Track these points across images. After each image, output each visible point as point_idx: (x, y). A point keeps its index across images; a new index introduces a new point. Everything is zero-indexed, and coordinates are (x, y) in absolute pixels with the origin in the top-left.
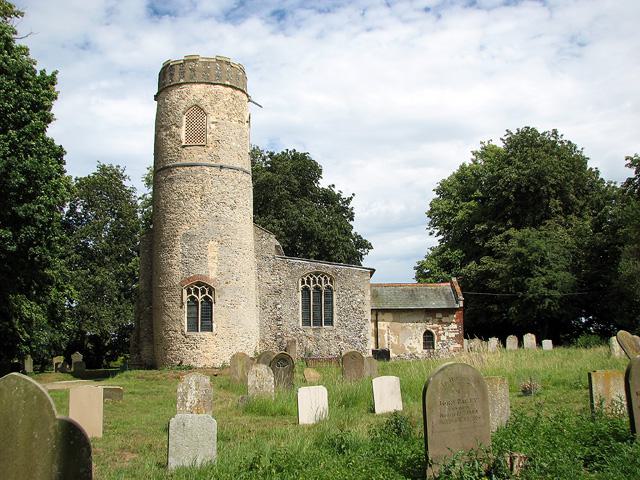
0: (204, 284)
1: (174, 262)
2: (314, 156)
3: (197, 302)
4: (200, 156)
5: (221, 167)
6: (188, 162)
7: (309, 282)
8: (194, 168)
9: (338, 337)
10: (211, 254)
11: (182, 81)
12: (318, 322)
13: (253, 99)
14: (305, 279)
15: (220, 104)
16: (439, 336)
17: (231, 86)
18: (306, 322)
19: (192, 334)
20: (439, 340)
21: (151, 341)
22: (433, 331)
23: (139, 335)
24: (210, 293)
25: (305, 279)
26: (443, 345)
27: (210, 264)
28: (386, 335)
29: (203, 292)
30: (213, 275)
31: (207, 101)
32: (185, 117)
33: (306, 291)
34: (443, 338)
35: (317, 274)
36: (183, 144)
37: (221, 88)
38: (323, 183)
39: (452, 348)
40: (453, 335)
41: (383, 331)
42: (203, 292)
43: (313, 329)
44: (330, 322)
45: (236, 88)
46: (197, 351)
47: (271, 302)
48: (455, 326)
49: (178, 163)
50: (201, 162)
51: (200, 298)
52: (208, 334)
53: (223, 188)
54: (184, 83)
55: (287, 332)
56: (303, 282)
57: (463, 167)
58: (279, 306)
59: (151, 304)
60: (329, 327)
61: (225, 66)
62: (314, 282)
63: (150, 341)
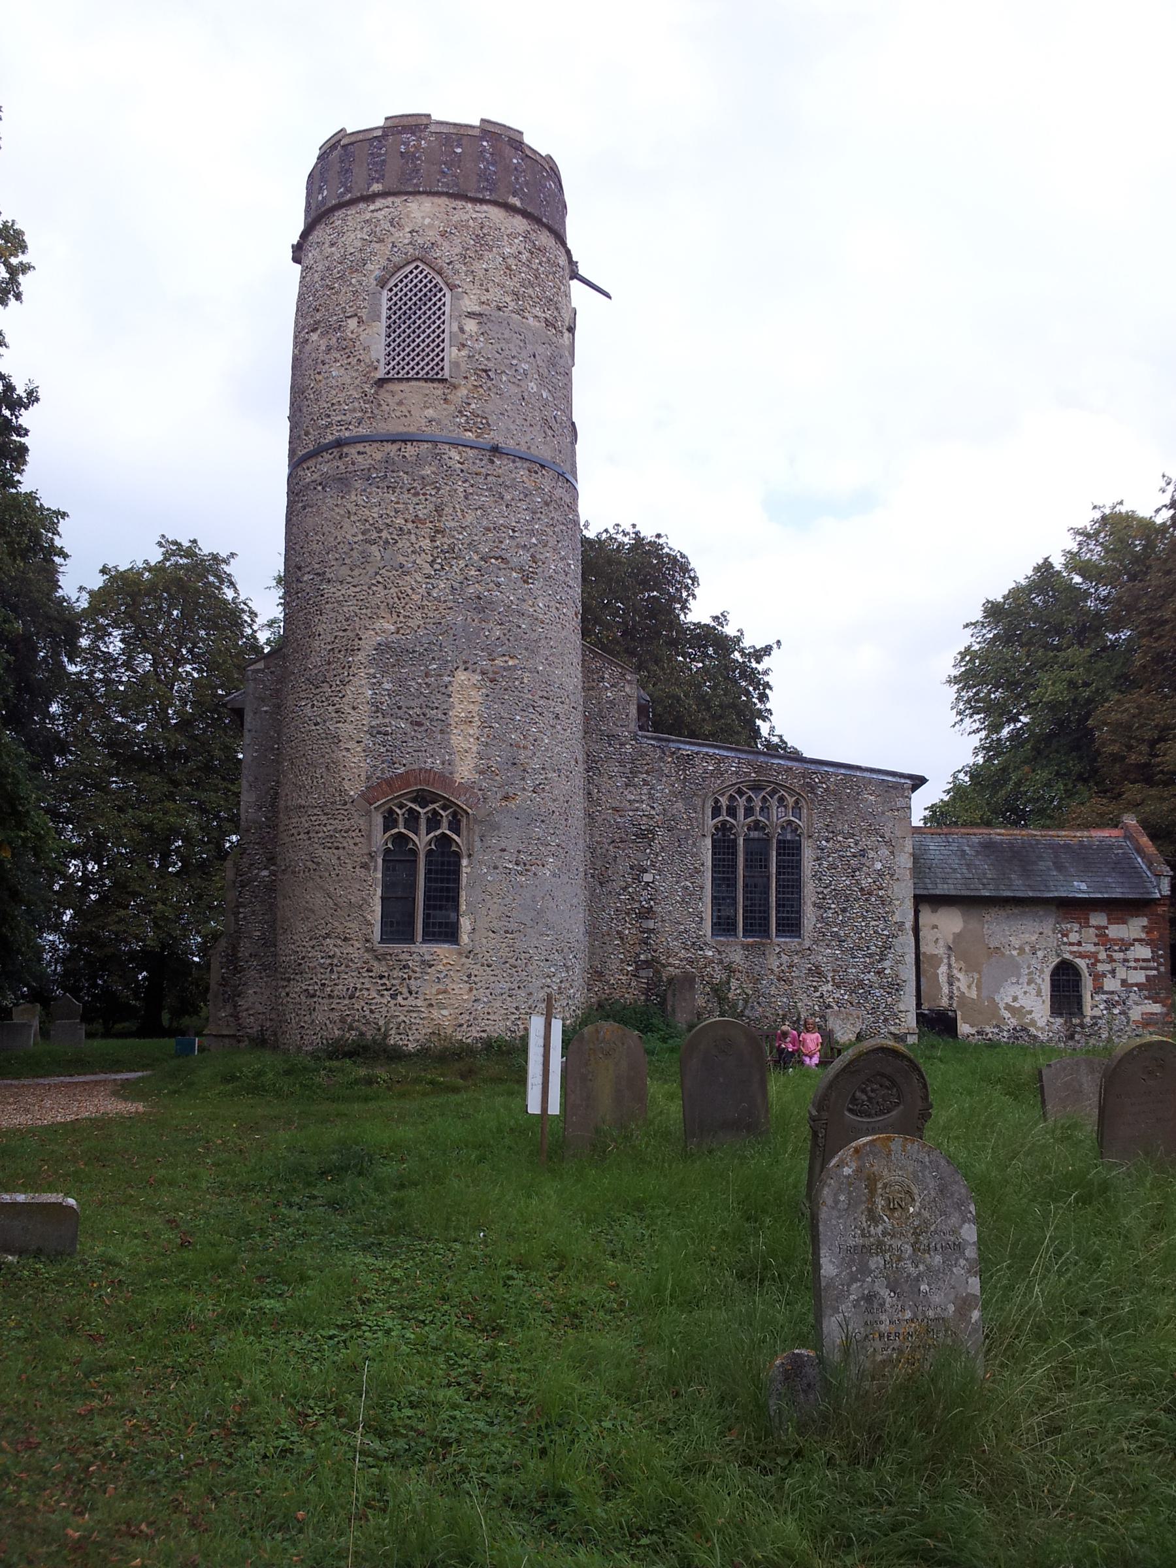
0: (435, 798)
1: (346, 729)
2: (675, 543)
3: (414, 852)
4: (430, 413)
5: (495, 450)
6: (395, 427)
7: (732, 811)
8: (410, 450)
9: (817, 972)
10: (459, 710)
11: (376, 187)
12: (757, 925)
13: (582, 271)
14: (724, 801)
15: (492, 261)
16: (1098, 977)
17: (525, 214)
18: (723, 926)
19: (396, 948)
20: (1099, 989)
21: (271, 968)
22: (1082, 963)
23: (235, 948)
24: (455, 826)
25: (724, 801)
26: (1111, 1006)
27: (457, 740)
28: (943, 970)
29: (434, 821)
30: (465, 771)
31: (447, 252)
32: (385, 294)
33: (724, 846)
34: (1110, 984)
35: (757, 787)
36: (380, 374)
37: (495, 213)
38: (698, 612)
39: (1136, 1014)
40: (1139, 977)
41: (935, 957)
42: (434, 821)
43: (746, 947)
44: (791, 925)
45: (538, 221)
46: (411, 1001)
47: (623, 866)
48: (1145, 952)
49: (362, 431)
50: (433, 431)
51: (422, 840)
52: (443, 950)
53: (497, 514)
54: (384, 194)
55: (669, 953)
56: (716, 811)
57: (1045, 568)
58: (648, 877)
59: (272, 860)
60: (793, 943)
61: (508, 150)
62: (749, 811)
63: (265, 967)
